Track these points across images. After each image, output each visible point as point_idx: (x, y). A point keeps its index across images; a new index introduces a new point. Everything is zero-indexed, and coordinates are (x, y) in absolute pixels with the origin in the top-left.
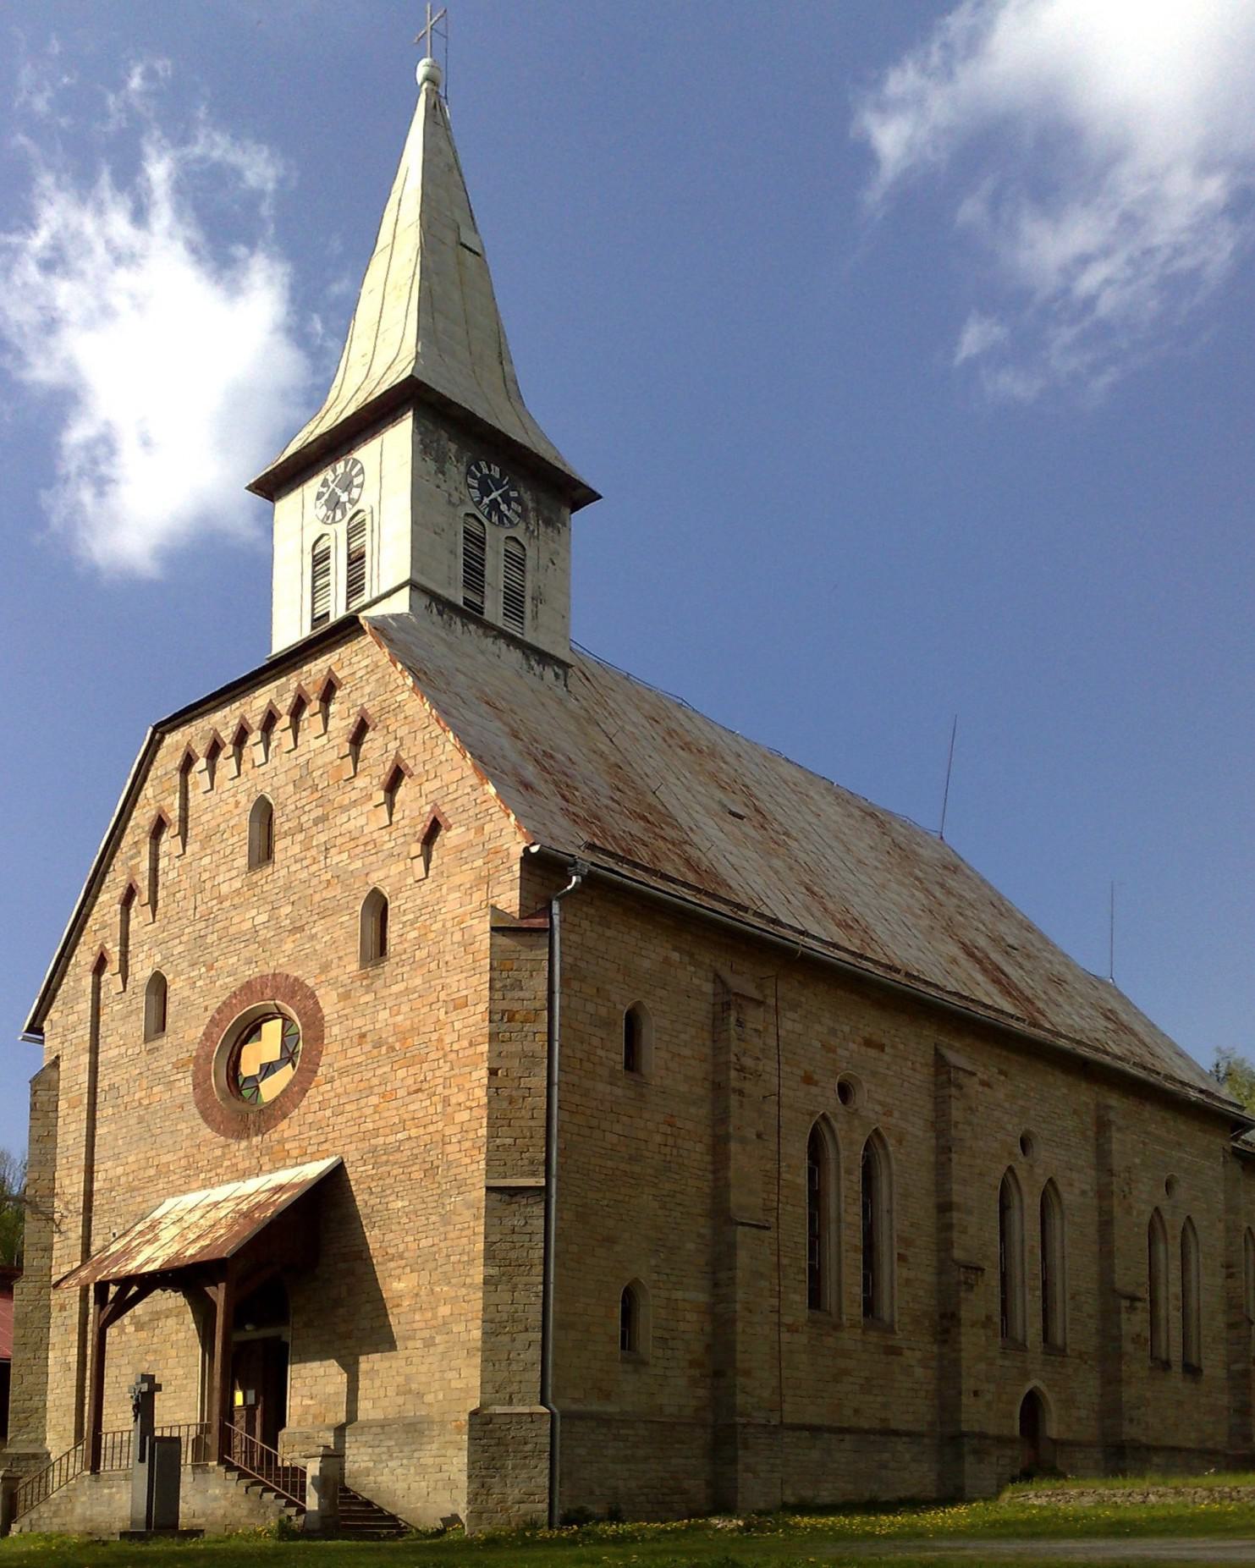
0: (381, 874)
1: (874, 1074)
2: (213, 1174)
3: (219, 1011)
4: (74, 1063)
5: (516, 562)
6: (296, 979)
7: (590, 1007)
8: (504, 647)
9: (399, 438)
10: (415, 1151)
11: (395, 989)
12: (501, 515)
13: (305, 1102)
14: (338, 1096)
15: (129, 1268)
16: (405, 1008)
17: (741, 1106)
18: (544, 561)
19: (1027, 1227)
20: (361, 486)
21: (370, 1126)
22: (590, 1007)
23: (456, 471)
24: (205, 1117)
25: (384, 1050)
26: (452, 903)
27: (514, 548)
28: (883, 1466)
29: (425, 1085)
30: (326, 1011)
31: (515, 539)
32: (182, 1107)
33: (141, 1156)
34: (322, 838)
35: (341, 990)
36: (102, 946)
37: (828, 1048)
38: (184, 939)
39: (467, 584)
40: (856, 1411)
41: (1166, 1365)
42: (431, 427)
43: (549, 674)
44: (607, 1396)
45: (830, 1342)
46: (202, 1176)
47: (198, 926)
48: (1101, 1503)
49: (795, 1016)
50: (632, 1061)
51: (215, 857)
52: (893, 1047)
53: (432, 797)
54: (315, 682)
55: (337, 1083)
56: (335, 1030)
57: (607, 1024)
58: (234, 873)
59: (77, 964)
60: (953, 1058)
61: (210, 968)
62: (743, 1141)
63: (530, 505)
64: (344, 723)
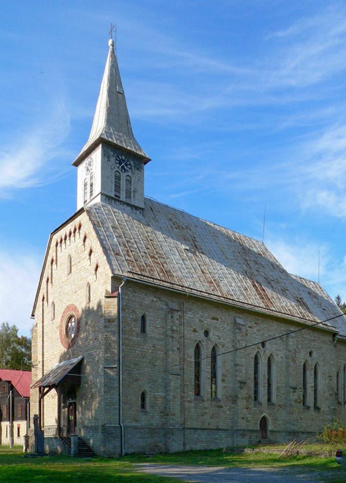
1: (215, 327)
5: (129, 181)
7: (131, 316)
8: (126, 207)
9: (98, 152)
12: (125, 169)
17: (172, 340)
18: (137, 180)
19: (263, 368)
22: (131, 316)
23: (113, 159)
27: (128, 178)
28: (217, 439)
31: (129, 176)
37: (201, 321)
39: (116, 191)
40: (208, 424)
41: (309, 408)
42: (106, 148)
43: (138, 212)
44: (137, 421)
45: (201, 405)
48: (311, 448)
49: (191, 313)
50: (143, 330)
52: (222, 319)
57: (135, 320)
60: (239, 321)
62: (173, 351)
63: (133, 165)
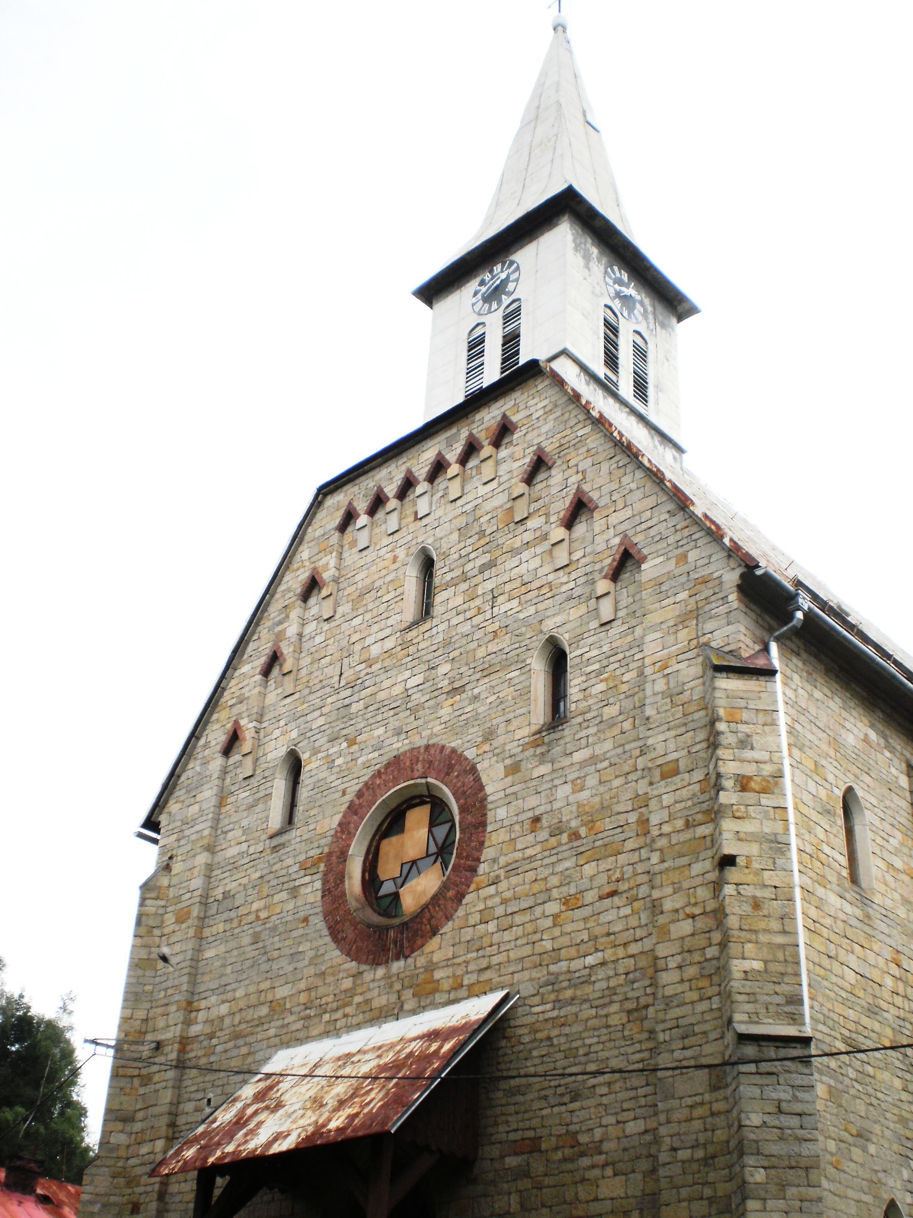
0: (559, 619)
2: (339, 1014)
3: (359, 795)
4: (189, 864)
5: (641, 354)
6: (454, 751)
10: (612, 983)
11: (578, 757)
13: (461, 912)
14: (504, 902)
15: (251, 1145)
16: (592, 781)
20: (517, 280)
21: (548, 945)
24: (335, 933)
25: (564, 838)
26: (654, 647)
29: (622, 887)
30: (489, 790)
32: (306, 920)
33: (252, 989)
34: (489, 585)
35: (508, 762)
36: (236, 722)
38: (325, 710)
46: (326, 1017)
47: (344, 694)
51: (368, 616)
53: (622, 528)
54: (487, 429)
55: (503, 885)
56: (502, 813)
58: (388, 632)
59: (206, 746)
61: (352, 742)
64: (520, 463)
